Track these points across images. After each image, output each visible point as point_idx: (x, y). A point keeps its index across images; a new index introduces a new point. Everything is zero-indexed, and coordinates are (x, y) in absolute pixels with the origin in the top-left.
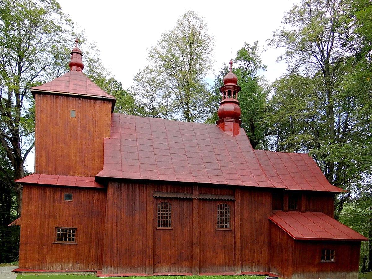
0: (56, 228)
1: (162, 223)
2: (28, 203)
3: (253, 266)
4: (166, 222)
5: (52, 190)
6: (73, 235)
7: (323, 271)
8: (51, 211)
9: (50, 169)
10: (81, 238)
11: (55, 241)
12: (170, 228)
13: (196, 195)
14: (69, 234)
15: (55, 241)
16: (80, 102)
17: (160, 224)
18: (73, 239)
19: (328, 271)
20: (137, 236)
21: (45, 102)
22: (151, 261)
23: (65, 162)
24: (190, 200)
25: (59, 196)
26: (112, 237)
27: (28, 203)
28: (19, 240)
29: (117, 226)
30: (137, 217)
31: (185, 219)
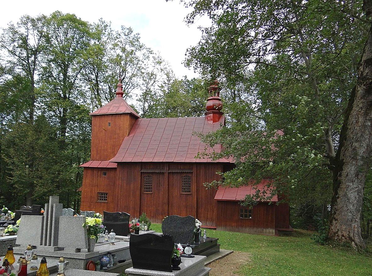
0: (98, 192)
1: (148, 189)
2: (86, 178)
3: (208, 222)
4: (149, 189)
5: (137, 167)
6: (106, 197)
7: (242, 226)
8: (96, 182)
9: (98, 158)
10: (110, 199)
11: (97, 201)
12: (151, 193)
13: (166, 170)
14: (249, 214)
15: (97, 201)
16: (114, 117)
17: (145, 190)
18: (106, 200)
19: (246, 227)
20: (132, 198)
21: (96, 120)
22: (138, 214)
23: (105, 154)
24: (163, 173)
25: (100, 174)
26: (118, 198)
27: (86, 178)
28: (281, 236)
29: (121, 191)
30: (132, 186)
31: (160, 186)
